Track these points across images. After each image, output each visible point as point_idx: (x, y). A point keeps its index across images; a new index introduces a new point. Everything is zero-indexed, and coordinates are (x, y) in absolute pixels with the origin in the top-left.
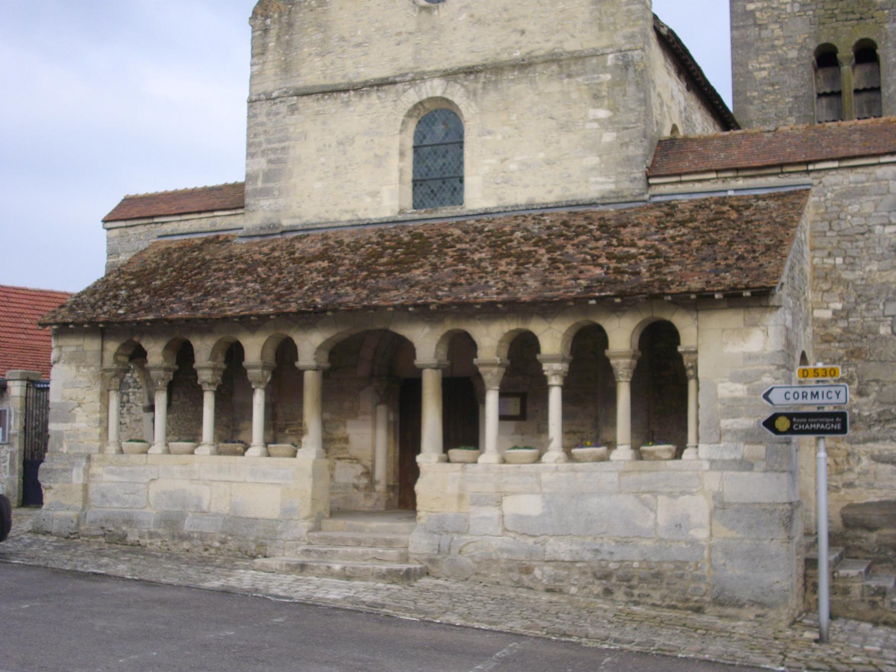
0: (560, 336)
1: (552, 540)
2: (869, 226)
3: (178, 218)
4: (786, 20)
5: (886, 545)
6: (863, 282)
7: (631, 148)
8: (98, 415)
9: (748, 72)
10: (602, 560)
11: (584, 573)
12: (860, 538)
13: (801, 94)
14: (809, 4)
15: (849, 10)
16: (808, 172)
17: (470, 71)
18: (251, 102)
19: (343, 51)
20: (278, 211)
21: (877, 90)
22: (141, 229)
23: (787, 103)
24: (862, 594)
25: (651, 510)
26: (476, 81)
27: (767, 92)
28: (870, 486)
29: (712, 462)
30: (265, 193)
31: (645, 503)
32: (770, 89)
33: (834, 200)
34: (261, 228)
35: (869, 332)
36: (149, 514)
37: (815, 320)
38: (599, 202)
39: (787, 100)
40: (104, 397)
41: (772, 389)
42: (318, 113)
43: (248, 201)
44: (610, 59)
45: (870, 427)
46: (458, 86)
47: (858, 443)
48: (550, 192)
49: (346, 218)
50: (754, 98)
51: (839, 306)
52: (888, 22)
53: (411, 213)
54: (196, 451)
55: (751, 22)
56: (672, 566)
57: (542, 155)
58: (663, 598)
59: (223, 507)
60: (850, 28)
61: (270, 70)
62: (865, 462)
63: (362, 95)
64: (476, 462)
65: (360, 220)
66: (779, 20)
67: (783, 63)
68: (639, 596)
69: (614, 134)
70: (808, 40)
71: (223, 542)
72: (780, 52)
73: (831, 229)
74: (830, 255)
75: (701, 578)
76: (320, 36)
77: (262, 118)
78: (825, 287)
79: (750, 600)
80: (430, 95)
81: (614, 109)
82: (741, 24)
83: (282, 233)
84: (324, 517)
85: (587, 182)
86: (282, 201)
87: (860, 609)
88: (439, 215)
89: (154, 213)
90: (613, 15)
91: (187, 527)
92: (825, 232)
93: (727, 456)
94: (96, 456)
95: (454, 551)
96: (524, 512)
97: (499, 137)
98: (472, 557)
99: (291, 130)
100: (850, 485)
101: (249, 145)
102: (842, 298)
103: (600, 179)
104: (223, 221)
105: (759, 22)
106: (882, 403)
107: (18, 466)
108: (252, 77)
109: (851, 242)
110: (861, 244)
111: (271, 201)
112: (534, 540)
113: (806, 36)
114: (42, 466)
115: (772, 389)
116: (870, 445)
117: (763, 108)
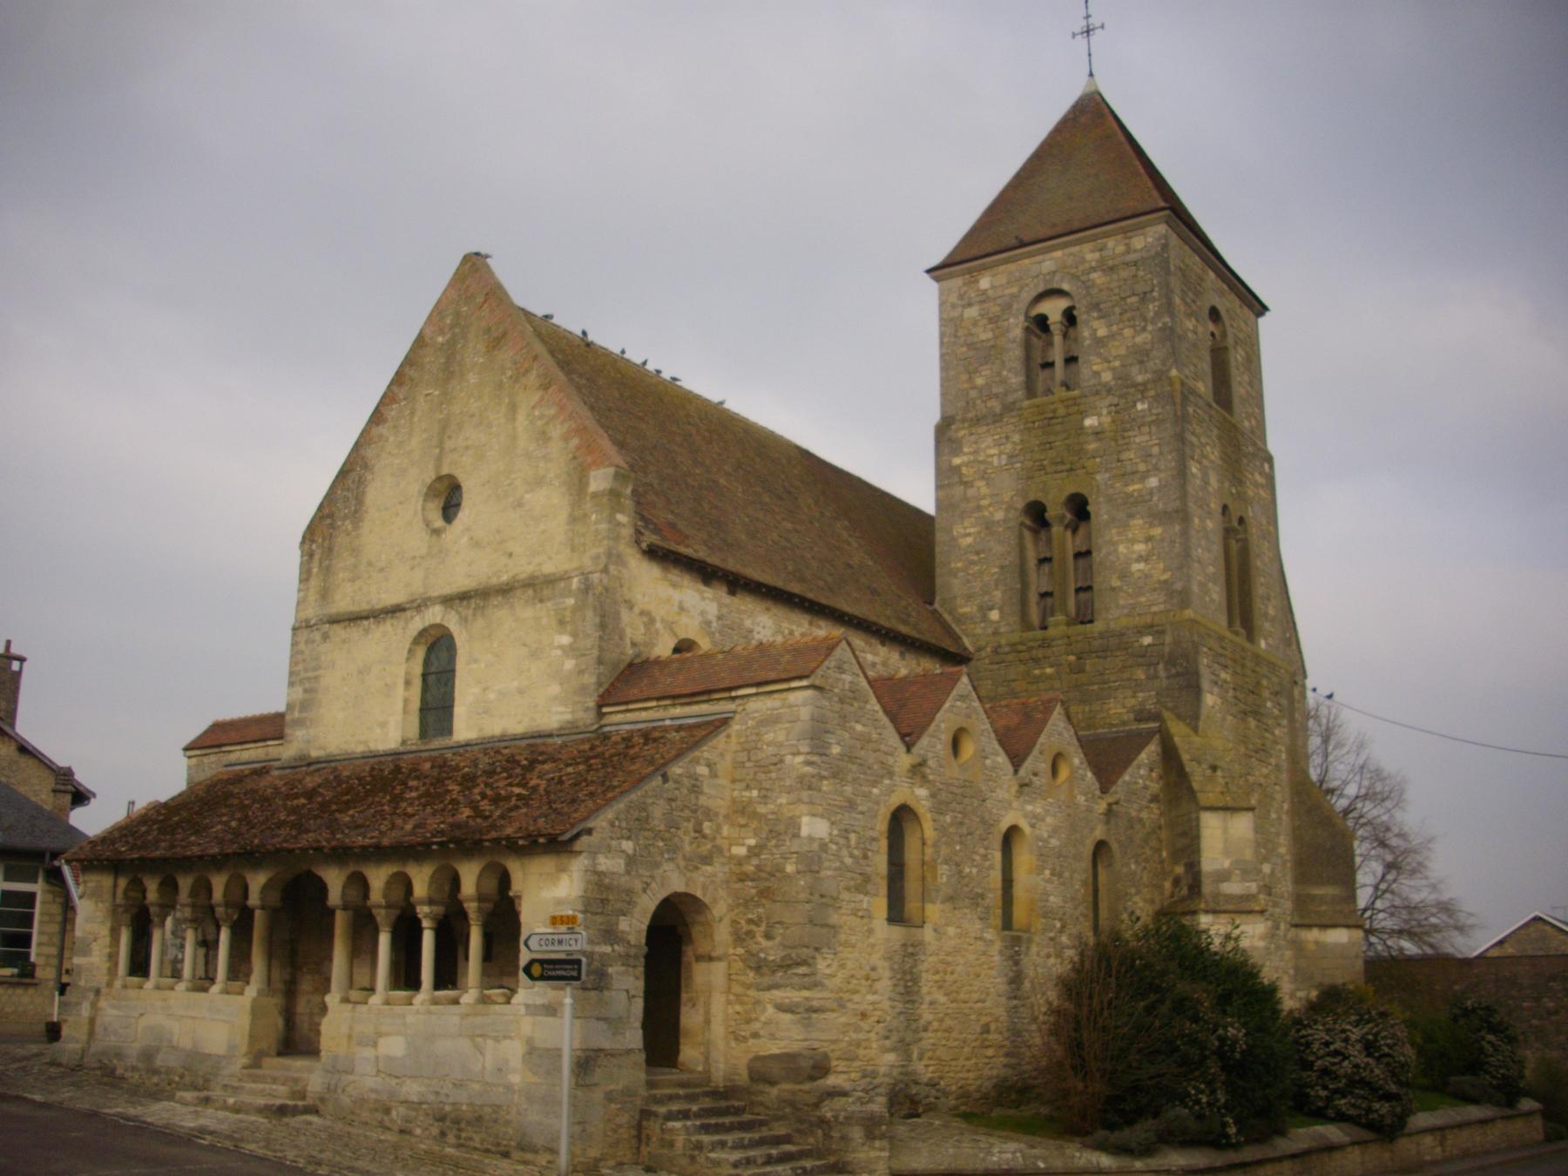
0: (427, 879)
1: (408, 1082)
2: (782, 756)
3: (239, 747)
4: (993, 476)
5: (784, 1101)
6: (774, 817)
7: (586, 676)
8: (108, 950)
10: (441, 1102)
11: (427, 1115)
12: (763, 1092)
13: (1007, 563)
14: (1017, 456)
15: (1059, 460)
16: (733, 698)
17: (464, 597)
18: (295, 629)
19: (370, 577)
20: (309, 742)
23: (993, 574)
24: (684, 1147)
25: (481, 1053)
26: (468, 607)
27: (973, 563)
28: (773, 1037)
29: (527, 1006)
30: (300, 723)
32: (975, 558)
33: (753, 728)
34: (295, 760)
35: (778, 871)
36: (134, 1049)
37: (732, 857)
38: (555, 732)
40: (115, 934)
41: (530, 937)
42: (344, 641)
43: (288, 731)
44: (575, 583)
45: (774, 972)
46: (453, 612)
47: (763, 990)
48: (520, 722)
49: (360, 749)
50: (958, 570)
51: (752, 842)
52: (1099, 472)
54: (176, 988)
55: (956, 479)
56: (490, 1110)
57: (516, 684)
58: (482, 1141)
59: (186, 1043)
60: (1059, 481)
61: (313, 597)
62: (770, 1010)
63: (379, 622)
64: (366, 1003)
65: (371, 752)
66: (986, 476)
67: (988, 526)
68: (465, 1139)
69: (574, 662)
70: (1015, 498)
72: (986, 513)
73: (749, 760)
74: (748, 787)
75: (508, 1123)
76: (352, 560)
77: (302, 646)
78: (742, 821)
79: (543, 1146)
80: (432, 622)
81: (574, 635)
82: (946, 482)
83: (309, 764)
84: (268, 1055)
85: (549, 711)
86: (312, 732)
88: (432, 747)
90: (583, 535)
91: (159, 1061)
92: (743, 763)
93: (539, 1001)
94: (104, 991)
95: (339, 1091)
97: (483, 665)
98: (350, 1096)
99: (323, 658)
100: (755, 1035)
101: (291, 674)
102: (756, 833)
104: (272, 750)
105: (965, 479)
106: (785, 947)
108: (298, 603)
109: (764, 773)
110: (773, 775)
111: (304, 732)
112: (397, 1081)
113: (1013, 493)
115: (530, 937)
117: (968, 581)
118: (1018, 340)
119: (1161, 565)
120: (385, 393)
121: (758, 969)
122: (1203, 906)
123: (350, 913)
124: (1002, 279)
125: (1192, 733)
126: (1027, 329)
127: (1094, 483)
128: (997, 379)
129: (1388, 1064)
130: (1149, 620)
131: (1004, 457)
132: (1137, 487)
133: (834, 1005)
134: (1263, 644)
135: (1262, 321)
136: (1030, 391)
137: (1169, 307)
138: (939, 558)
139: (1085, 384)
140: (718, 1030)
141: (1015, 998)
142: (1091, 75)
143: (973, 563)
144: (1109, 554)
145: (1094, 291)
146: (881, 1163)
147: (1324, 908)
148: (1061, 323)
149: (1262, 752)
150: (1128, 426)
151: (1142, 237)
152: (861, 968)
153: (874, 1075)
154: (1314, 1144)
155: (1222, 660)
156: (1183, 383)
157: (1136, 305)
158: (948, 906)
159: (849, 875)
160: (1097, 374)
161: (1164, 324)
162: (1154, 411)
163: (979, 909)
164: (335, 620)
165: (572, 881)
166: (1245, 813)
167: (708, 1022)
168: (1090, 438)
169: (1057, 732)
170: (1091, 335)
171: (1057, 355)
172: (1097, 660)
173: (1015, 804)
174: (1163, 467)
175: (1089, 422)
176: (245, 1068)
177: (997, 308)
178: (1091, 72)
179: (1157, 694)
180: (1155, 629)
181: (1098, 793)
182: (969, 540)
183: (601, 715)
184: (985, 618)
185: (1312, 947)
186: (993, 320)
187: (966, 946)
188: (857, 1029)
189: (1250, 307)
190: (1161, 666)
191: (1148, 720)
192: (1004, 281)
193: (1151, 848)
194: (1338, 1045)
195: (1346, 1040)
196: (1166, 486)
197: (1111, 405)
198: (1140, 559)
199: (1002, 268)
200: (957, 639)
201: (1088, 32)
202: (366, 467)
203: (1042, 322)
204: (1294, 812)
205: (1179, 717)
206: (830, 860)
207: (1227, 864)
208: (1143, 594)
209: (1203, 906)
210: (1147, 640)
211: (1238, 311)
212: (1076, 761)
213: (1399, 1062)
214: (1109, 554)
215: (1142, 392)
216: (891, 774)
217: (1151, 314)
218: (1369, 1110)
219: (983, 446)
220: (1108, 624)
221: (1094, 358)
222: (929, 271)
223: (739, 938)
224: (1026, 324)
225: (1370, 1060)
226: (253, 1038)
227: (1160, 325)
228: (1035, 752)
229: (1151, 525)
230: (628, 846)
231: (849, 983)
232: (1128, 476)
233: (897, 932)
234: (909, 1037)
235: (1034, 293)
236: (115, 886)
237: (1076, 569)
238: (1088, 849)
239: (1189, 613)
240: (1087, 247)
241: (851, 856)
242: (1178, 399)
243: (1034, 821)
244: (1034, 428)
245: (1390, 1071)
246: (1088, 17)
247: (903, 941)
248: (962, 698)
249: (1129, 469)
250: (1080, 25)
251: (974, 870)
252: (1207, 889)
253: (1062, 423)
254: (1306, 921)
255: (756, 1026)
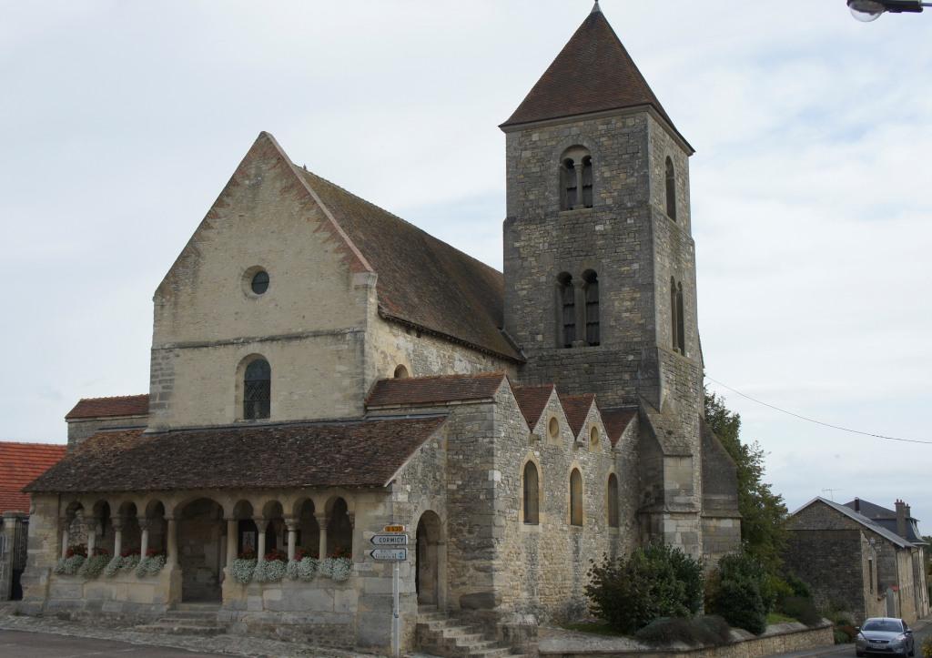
0: (292, 505)
8: (56, 545)
9: (515, 291)
16: (447, 406)
17: (272, 339)
21: (596, 303)
22: (89, 424)
27: (527, 306)
28: (474, 584)
30: (161, 406)
31: (329, 594)
32: (528, 303)
37: (448, 490)
39: (540, 311)
43: (151, 411)
45: (474, 551)
48: (315, 413)
53: (242, 421)
59: (123, 597)
62: (472, 571)
67: (537, 285)
71: (122, 617)
74: (457, 454)
78: (454, 471)
83: (170, 431)
87: (41, 579)
89: (96, 414)
91: (104, 608)
96: (273, 599)
103: (340, 407)
106: (480, 538)
107: (9, 573)
110: (472, 448)
114: (23, 574)
116: (474, 561)
120: (210, 212)
121: (464, 549)
123: (237, 523)
126: (561, 168)
131: (546, 244)
132: (626, 268)
140: (443, 582)
141: (576, 561)
144: (609, 306)
160: (604, 199)
164: (183, 346)
165: (386, 507)
167: (436, 576)
168: (599, 237)
169: (593, 416)
171: (578, 184)
175: (598, 228)
176: (168, 610)
182: (525, 292)
183: (366, 411)
184: (534, 340)
186: (541, 160)
189: (685, 151)
191: (630, 403)
192: (547, 137)
202: (198, 254)
203: (569, 164)
207: (678, 486)
214: (609, 306)
219: (533, 237)
223: (452, 533)
226: (171, 593)
229: (634, 291)
230: (408, 487)
232: (624, 261)
234: (533, 583)
235: (566, 147)
236: (60, 506)
237: (587, 311)
238: (606, 479)
240: (599, 122)
248: (553, 401)
249: (622, 258)
255: (464, 579)
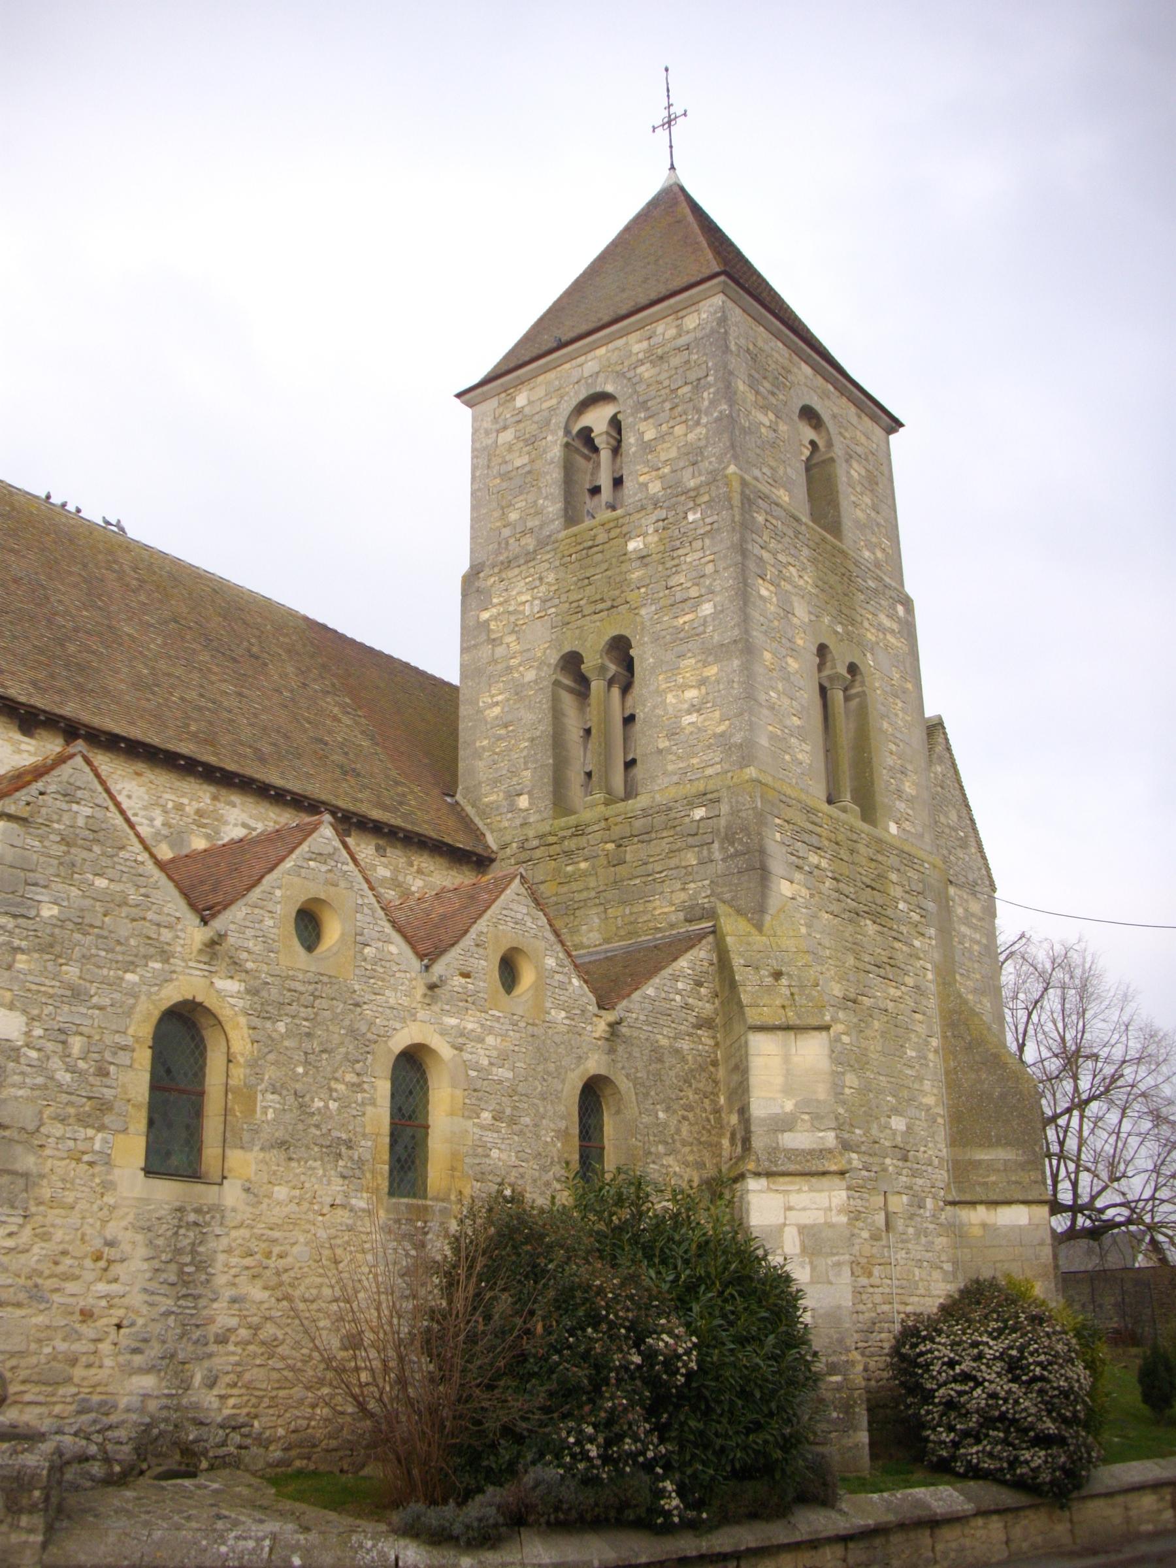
13: (538, 733)
15: (598, 597)
27: (500, 738)
105: (493, 636)
113: (546, 645)
118: (556, 460)
119: (717, 714)
122: (751, 1166)
124: (540, 392)
125: (753, 931)
127: (638, 619)
128: (532, 511)
129: (1041, 1392)
130: (701, 786)
131: (537, 602)
132: (687, 618)
133: (22, 1296)
134: (893, 828)
135: (893, 438)
136: (571, 517)
137: (728, 392)
138: (463, 736)
139: (630, 501)
142: (672, 167)
143: (500, 738)
144: (655, 707)
145: (641, 388)
146: (28, 1552)
147: (993, 1178)
148: (607, 433)
149: (889, 968)
150: (678, 543)
151: (696, 314)
152: (83, 1239)
153: (106, 1407)
154: (891, 1518)
155: (814, 840)
156: (744, 483)
157: (689, 395)
158: (275, 1155)
159: (64, 1098)
161: (721, 412)
162: (708, 520)
163: (341, 1163)
166: (815, 1033)
170: (637, 440)
172: (640, 845)
173: (421, 1015)
174: (718, 589)
177: (535, 426)
178: (672, 165)
179: (712, 882)
180: (709, 796)
181: (593, 1008)
182: (497, 710)
184: (513, 808)
185: (977, 1231)
187: (311, 1216)
188: (71, 1335)
190: (716, 845)
193: (697, 1091)
194: (966, 1366)
195: (979, 1357)
196: (722, 611)
197: (658, 521)
198: (694, 708)
199: (541, 379)
200: (479, 836)
201: (669, 122)
203: (586, 435)
204: (948, 1051)
205: (739, 912)
206: (22, 1073)
207: (789, 1106)
208: (695, 755)
209: (751, 1166)
210: (699, 813)
211: (854, 420)
212: (550, 962)
213: (1058, 1388)
214: (655, 707)
215: (694, 499)
216: (165, 955)
217: (706, 403)
218: (1014, 1463)
219: (514, 593)
220: (653, 798)
221: (641, 468)
222: (459, 396)
224: (565, 440)
225: (1014, 1387)
227: (716, 414)
228: (468, 941)
229: (706, 664)
231: (56, 1263)
233: (166, 1191)
235: (574, 402)
239: (751, 772)
241: (71, 1069)
242: (736, 500)
243: (460, 1040)
244: (571, 563)
245: (1046, 1403)
246: (670, 106)
247: (177, 1204)
250: (661, 115)
251: (333, 1105)
252: (759, 1142)
253: (602, 552)
254: (968, 1197)
